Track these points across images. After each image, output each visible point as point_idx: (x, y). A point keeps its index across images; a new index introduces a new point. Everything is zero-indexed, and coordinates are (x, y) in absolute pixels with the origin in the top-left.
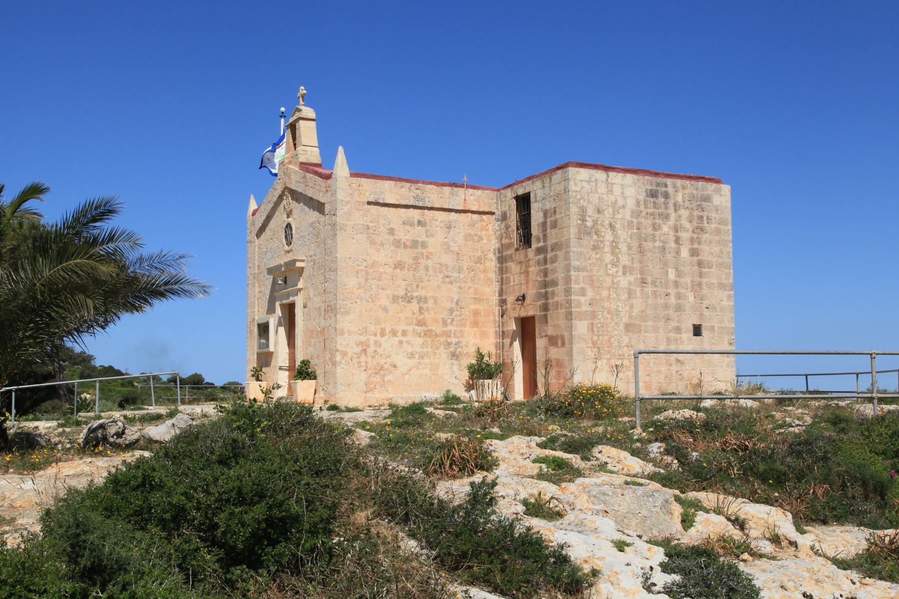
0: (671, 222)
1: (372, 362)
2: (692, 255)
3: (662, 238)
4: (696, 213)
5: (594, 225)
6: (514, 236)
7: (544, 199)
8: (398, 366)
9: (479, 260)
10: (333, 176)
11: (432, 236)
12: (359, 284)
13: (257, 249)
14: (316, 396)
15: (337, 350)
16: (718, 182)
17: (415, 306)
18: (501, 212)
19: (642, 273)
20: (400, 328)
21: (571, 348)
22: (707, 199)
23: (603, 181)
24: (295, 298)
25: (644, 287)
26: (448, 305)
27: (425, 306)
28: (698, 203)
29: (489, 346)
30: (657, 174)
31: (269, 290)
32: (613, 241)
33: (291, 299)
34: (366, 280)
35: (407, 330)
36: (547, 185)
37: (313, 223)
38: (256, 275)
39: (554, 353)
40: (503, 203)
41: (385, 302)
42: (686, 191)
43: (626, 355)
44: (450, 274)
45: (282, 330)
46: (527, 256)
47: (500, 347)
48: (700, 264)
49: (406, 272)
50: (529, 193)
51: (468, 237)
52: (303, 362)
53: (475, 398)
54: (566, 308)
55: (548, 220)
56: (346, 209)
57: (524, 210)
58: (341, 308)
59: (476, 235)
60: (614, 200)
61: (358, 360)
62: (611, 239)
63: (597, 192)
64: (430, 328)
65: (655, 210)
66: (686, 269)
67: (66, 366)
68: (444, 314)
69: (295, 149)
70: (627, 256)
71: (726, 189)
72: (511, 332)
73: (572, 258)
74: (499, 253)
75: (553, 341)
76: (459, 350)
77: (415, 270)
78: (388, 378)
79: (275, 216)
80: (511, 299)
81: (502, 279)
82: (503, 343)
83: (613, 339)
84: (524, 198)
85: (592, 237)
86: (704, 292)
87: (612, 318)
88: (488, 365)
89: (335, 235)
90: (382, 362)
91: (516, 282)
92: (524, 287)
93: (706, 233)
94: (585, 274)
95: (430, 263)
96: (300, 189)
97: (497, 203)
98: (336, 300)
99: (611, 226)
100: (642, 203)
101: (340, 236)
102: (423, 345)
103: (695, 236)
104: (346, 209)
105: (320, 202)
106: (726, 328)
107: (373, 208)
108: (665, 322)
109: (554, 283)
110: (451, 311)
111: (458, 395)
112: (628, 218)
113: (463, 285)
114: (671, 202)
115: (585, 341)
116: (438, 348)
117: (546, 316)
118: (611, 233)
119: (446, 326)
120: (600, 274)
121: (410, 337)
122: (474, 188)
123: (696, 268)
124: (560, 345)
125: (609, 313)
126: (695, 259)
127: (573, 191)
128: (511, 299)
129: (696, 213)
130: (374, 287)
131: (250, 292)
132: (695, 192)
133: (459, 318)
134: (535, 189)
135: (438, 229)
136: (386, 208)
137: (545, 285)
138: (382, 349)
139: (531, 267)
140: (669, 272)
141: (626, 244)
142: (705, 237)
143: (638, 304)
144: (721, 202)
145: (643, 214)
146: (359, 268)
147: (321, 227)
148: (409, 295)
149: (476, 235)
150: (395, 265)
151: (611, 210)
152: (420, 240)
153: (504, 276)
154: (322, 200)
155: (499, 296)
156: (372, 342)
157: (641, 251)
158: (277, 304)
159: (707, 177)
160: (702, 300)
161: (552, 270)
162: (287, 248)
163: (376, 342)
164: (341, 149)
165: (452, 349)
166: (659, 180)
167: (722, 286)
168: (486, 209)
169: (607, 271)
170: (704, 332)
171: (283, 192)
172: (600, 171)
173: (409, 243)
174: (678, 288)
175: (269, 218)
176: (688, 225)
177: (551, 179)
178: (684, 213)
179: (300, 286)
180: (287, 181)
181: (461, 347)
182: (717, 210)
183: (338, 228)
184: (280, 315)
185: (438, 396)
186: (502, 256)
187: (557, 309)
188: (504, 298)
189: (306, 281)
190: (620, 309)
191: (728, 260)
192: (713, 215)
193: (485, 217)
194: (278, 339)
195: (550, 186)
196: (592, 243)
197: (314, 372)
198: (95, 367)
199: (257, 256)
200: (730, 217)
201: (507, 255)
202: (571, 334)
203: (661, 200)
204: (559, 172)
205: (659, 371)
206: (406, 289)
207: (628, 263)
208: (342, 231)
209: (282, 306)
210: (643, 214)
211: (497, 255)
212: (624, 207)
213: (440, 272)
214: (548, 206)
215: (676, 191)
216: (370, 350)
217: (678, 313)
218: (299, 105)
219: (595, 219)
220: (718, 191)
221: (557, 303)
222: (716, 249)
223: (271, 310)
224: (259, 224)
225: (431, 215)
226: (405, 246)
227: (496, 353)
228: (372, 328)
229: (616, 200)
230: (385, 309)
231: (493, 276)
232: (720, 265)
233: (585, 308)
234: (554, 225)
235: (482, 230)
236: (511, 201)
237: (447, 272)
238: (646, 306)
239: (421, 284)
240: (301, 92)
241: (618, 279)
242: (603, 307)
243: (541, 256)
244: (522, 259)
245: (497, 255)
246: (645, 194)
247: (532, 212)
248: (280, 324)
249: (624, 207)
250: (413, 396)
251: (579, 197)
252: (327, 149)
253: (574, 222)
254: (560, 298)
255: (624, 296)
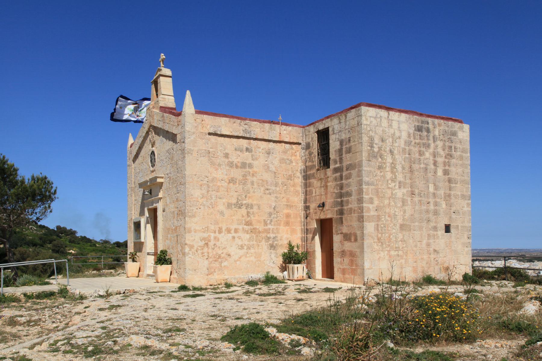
0: (431, 150)
1: (212, 252)
2: (445, 175)
3: (425, 162)
4: (447, 144)
5: (379, 151)
6: (316, 160)
7: (340, 131)
8: (232, 255)
9: (290, 178)
10: (183, 113)
11: (257, 159)
12: (203, 194)
13: (133, 171)
14: (172, 276)
15: (186, 244)
16: (461, 122)
17: (244, 211)
18: (306, 143)
19: (411, 187)
20: (233, 227)
21: (363, 243)
22: (454, 134)
23: (385, 118)
24: (157, 205)
25: (413, 197)
26: (268, 210)
27: (251, 211)
28: (449, 137)
29: (297, 239)
30: (421, 115)
31: (141, 198)
32: (392, 163)
33: (155, 205)
34: (208, 191)
35: (238, 229)
36: (343, 121)
37: (169, 150)
38: (133, 188)
39: (348, 246)
40: (307, 136)
41: (221, 208)
42: (442, 128)
43: (401, 247)
44: (269, 187)
45: (149, 226)
46: (326, 174)
47: (305, 240)
48: (450, 181)
49: (237, 185)
50: (328, 128)
51: (282, 161)
52: (162, 251)
53: (287, 277)
54: (359, 213)
55: (344, 147)
56: (192, 138)
57: (324, 140)
58: (188, 212)
59: (288, 159)
60: (393, 132)
61: (201, 251)
62: (391, 161)
63: (381, 126)
64: (255, 227)
65: (421, 141)
66: (441, 184)
67: (63, 236)
68: (265, 217)
69: (157, 97)
70: (401, 174)
71: (466, 127)
72: (313, 230)
73: (364, 175)
74: (304, 172)
75: (347, 237)
76: (276, 242)
77: (244, 184)
78: (225, 264)
79: (144, 147)
80: (313, 206)
81: (306, 191)
82: (306, 237)
83: (392, 236)
84: (323, 132)
85: (377, 159)
86: (452, 201)
87: (391, 220)
88: (297, 254)
89: (184, 157)
90: (220, 252)
91: (318, 193)
92: (323, 197)
93: (454, 158)
94: (373, 187)
95: (255, 179)
96: (160, 125)
97: (303, 137)
98: (185, 207)
99: (391, 152)
100: (412, 135)
101: (188, 158)
102: (250, 240)
103: (447, 160)
104: (192, 138)
105: (174, 134)
106: (465, 227)
107: (213, 138)
108: (427, 223)
109: (349, 194)
110: (270, 214)
111: (275, 275)
112: (403, 146)
113: (279, 195)
114: (431, 135)
115: (372, 237)
116: (260, 241)
117: (341, 218)
118: (390, 157)
119: (267, 225)
120: (383, 187)
121: (240, 234)
122: (287, 125)
123: (447, 183)
124: (353, 240)
125: (389, 216)
126: (447, 177)
127: (365, 125)
128: (313, 206)
129: (447, 144)
130: (213, 196)
131: (129, 200)
132: (447, 129)
133: (275, 219)
134: (333, 124)
135: (261, 154)
136: (223, 138)
137: (341, 195)
138: (220, 242)
139: (329, 182)
140: (430, 187)
141: (401, 165)
142: (453, 161)
143: (408, 209)
144: (463, 137)
145: (413, 143)
146: (202, 182)
147: (175, 153)
148: (239, 202)
149: (288, 159)
150: (229, 180)
151: (391, 140)
152: (248, 162)
153: (308, 189)
154: (175, 132)
155: (304, 204)
156: (212, 238)
157: (411, 171)
158: (146, 209)
159: (454, 118)
160: (451, 207)
161: (347, 184)
162: (152, 169)
163: (215, 238)
164: (188, 92)
165: (271, 242)
166: (424, 119)
167: (463, 197)
168: (295, 141)
169: (388, 185)
170: (452, 230)
171: (149, 129)
172: (383, 110)
173: (239, 165)
174: (435, 198)
175: (140, 148)
176: (442, 153)
177: (346, 116)
178: (440, 144)
179: (160, 195)
180: (152, 120)
181: (277, 241)
182: (461, 142)
183: (186, 152)
184: (148, 216)
185: (261, 277)
186: (306, 175)
187: (351, 213)
188: (308, 205)
189: (164, 193)
190: (397, 213)
191: (467, 178)
192: (458, 146)
193: (294, 146)
194: (146, 232)
195: (345, 122)
196: (378, 164)
197: (170, 259)
198: (77, 237)
199: (133, 175)
200: (469, 147)
201: (310, 174)
202: (363, 233)
203: (425, 133)
204: (353, 110)
205: (422, 259)
206: (238, 199)
207: (402, 179)
208: (189, 154)
209: (149, 210)
210: (413, 143)
211: (303, 174)
212: (399, 138)
213: (262, 186)
214: (344, 136)
215: (434, 127)
216: (211, 244)
217: (435, 216)
218: (160, 67)
219: (380, 146)
220: (461, 129)
221: (351, 209)
222: (460, 170)
223: (142, 213)
224: (134, 153)
225: (256, 144)
226: (237, 167)
227: (302, 244)
228: (212, 227)
229: (394, 133)
230: (222, 213)
231: (300, 189)
232: (463, 181)
233: (373, 213)
234: (349, 151)
235: (292, 156)
236: (313, 135)
237: (267, 186)
238: (414, 211)
239: (248, 195)
240: (161, 57)
241: (396, 191)
242: (385, 213)
243: (338, 174)
244: (322, 177)
245: (303, 174)
246: (414, 129)
247: (331, 141)
248: (147, 222)
249: (399, 138)
250: (242, 277)
251: (369, 129)
252: (179, 97)
253: (365, 147)
254: (353, 204)
255: (400, 204)
